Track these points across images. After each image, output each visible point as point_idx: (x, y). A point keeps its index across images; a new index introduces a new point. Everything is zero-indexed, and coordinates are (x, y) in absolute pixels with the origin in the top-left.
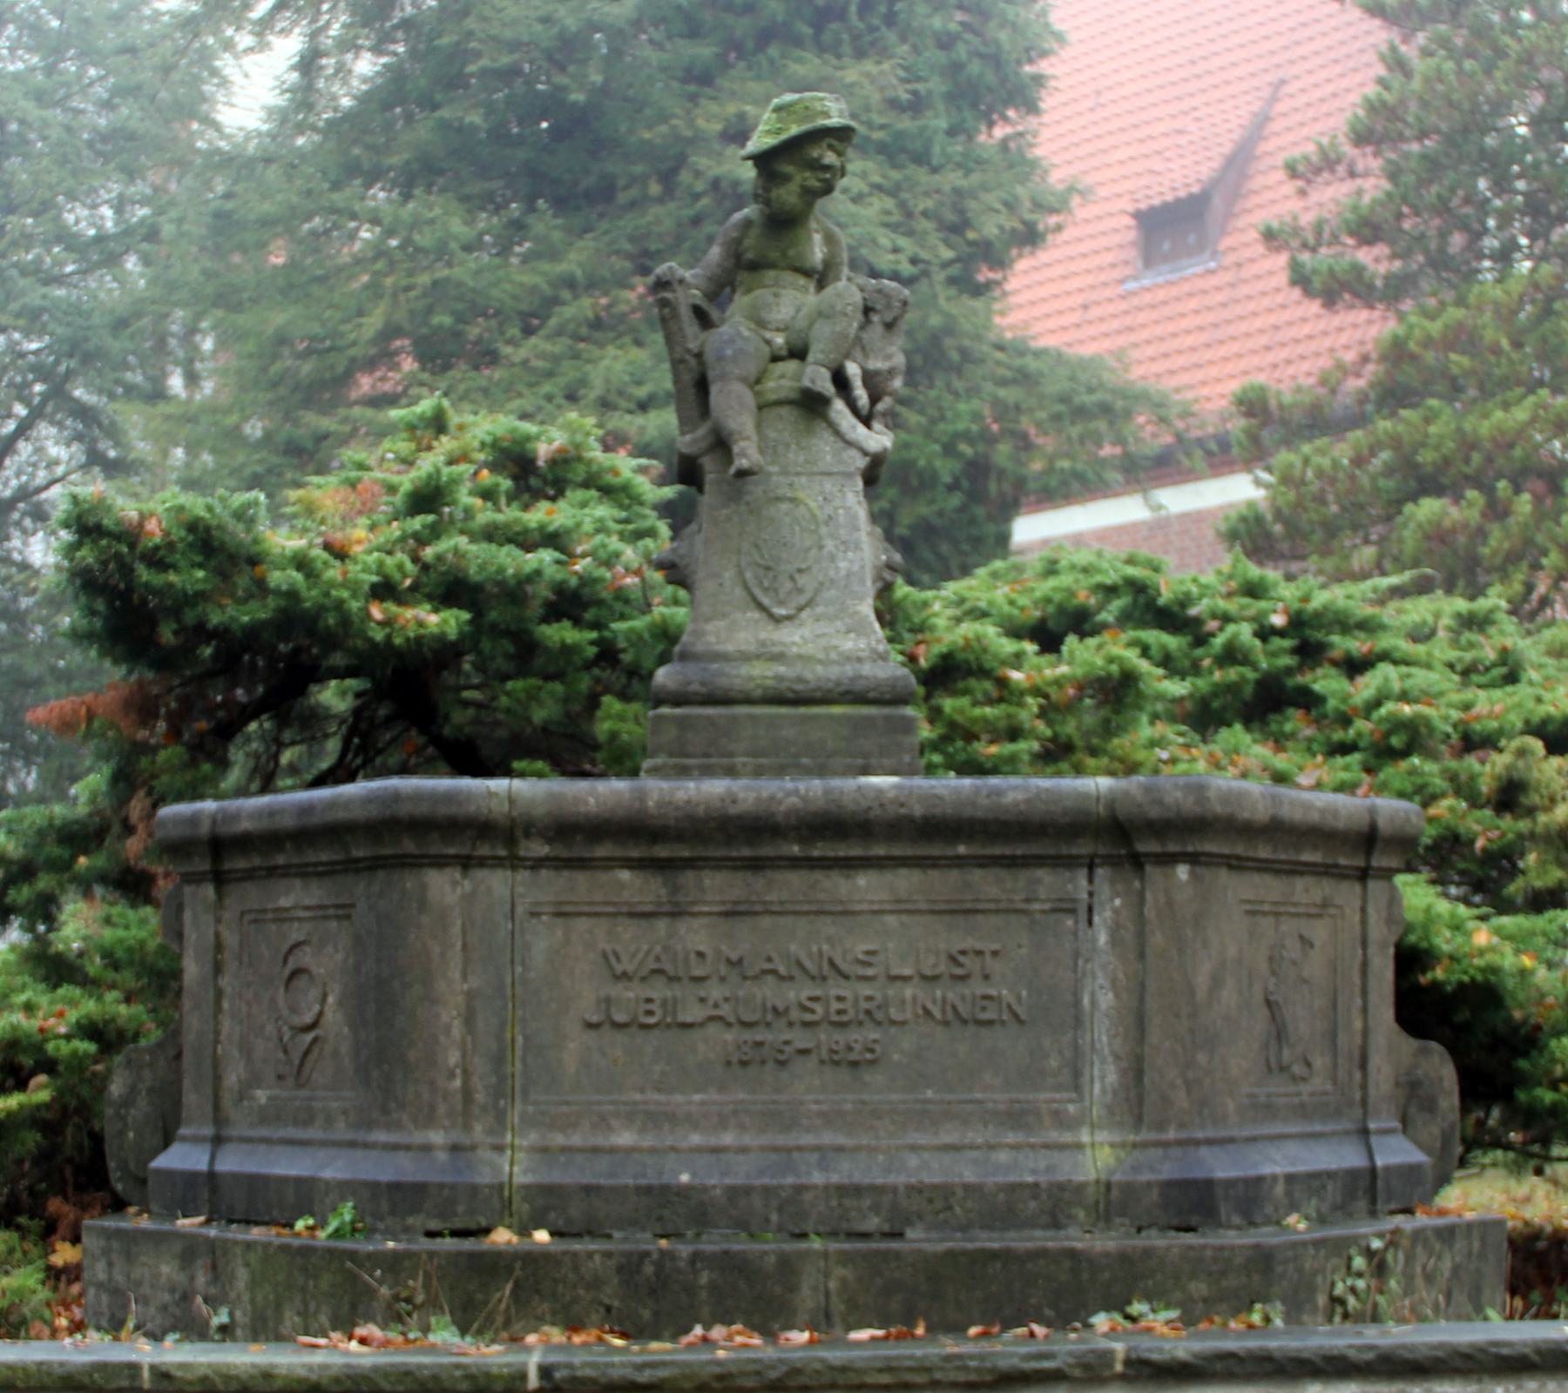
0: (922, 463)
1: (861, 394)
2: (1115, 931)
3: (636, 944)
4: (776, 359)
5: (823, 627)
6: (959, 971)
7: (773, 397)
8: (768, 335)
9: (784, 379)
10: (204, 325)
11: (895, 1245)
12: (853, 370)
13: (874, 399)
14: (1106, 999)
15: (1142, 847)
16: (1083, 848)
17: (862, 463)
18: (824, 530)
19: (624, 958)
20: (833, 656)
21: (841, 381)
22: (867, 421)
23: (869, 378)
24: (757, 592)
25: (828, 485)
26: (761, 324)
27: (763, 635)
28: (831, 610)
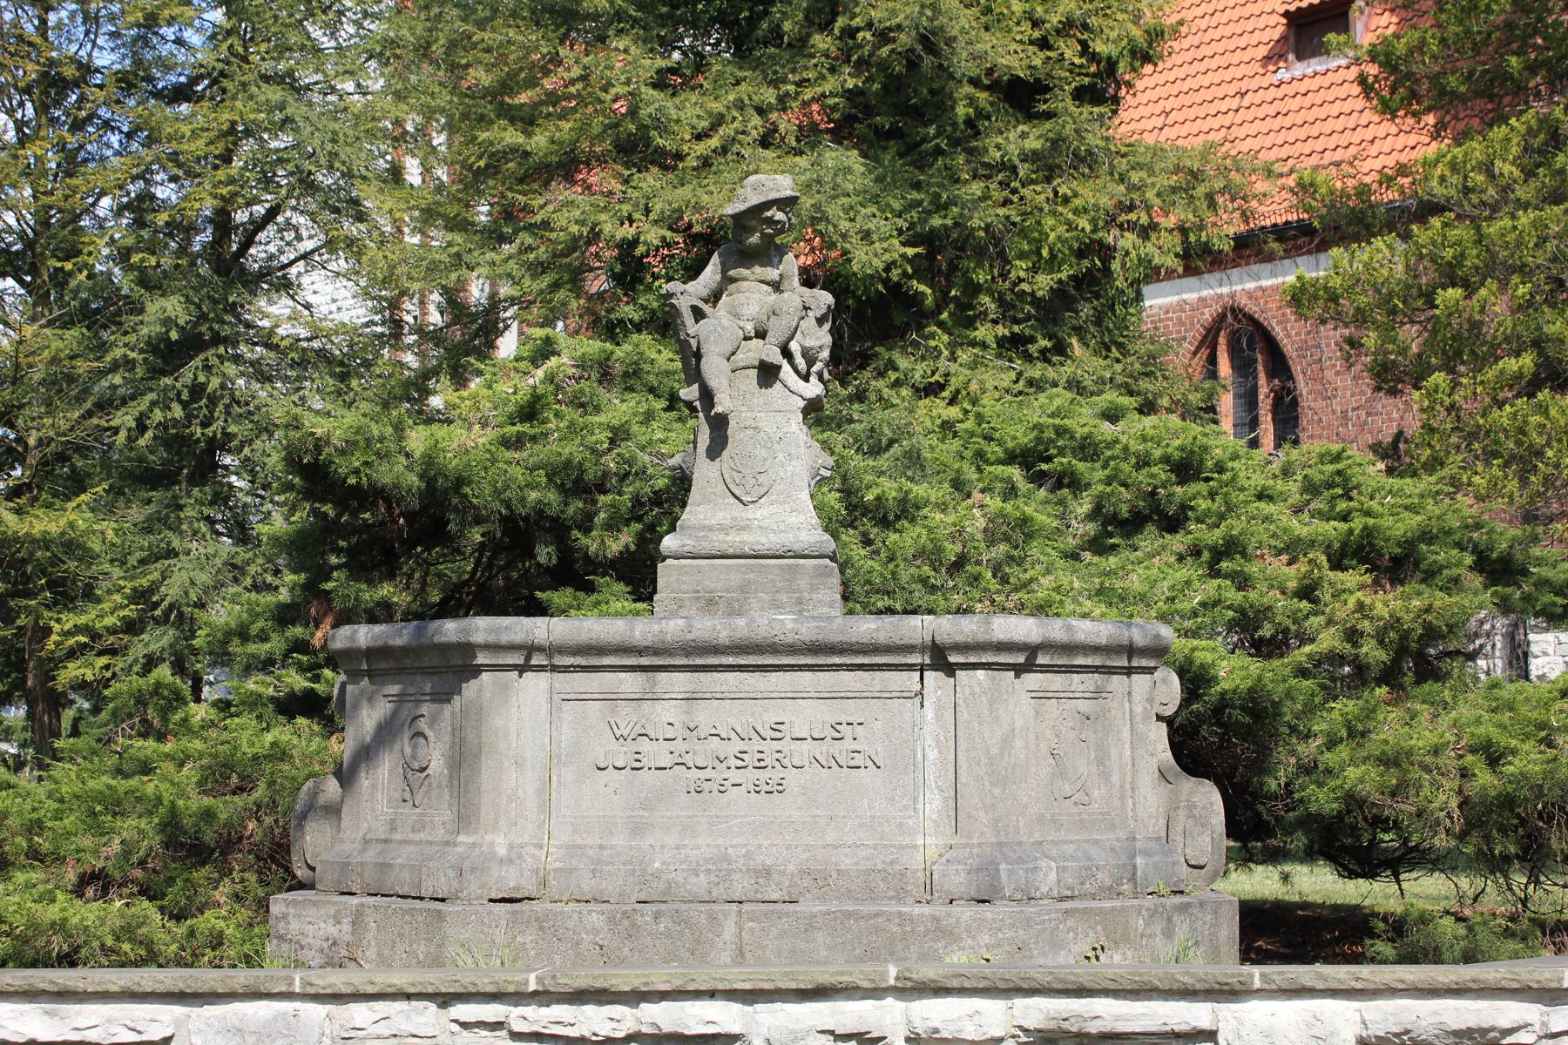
0: (158, 838)
1: (801, 362)
2: (939, 710)
3: (627, 717)
4: (746, 339)
5: (774, 509)
6: (838, 735)
7: (742, 364)
8: (741, 324)
9: (757, 350)
10: (611, 33)
11: (791, 907)
12: (794, 346)
13: (810, 363)
14: (932, 755)
15: (953, 659)
16: (915, 659)
17: (802, 404)
18: (776, 446)
19: (622, 726)
20: (782, 527)
21: (786, 353)
22: (806, 378)
23: (806, 353)
24: (732, 486)
25: (779, 417)
26: (737, 316)
27: (734, 514)
28: (781, 498)
